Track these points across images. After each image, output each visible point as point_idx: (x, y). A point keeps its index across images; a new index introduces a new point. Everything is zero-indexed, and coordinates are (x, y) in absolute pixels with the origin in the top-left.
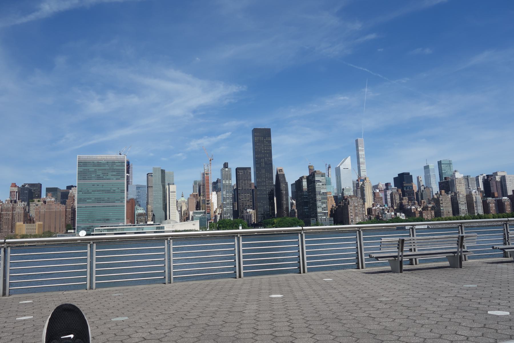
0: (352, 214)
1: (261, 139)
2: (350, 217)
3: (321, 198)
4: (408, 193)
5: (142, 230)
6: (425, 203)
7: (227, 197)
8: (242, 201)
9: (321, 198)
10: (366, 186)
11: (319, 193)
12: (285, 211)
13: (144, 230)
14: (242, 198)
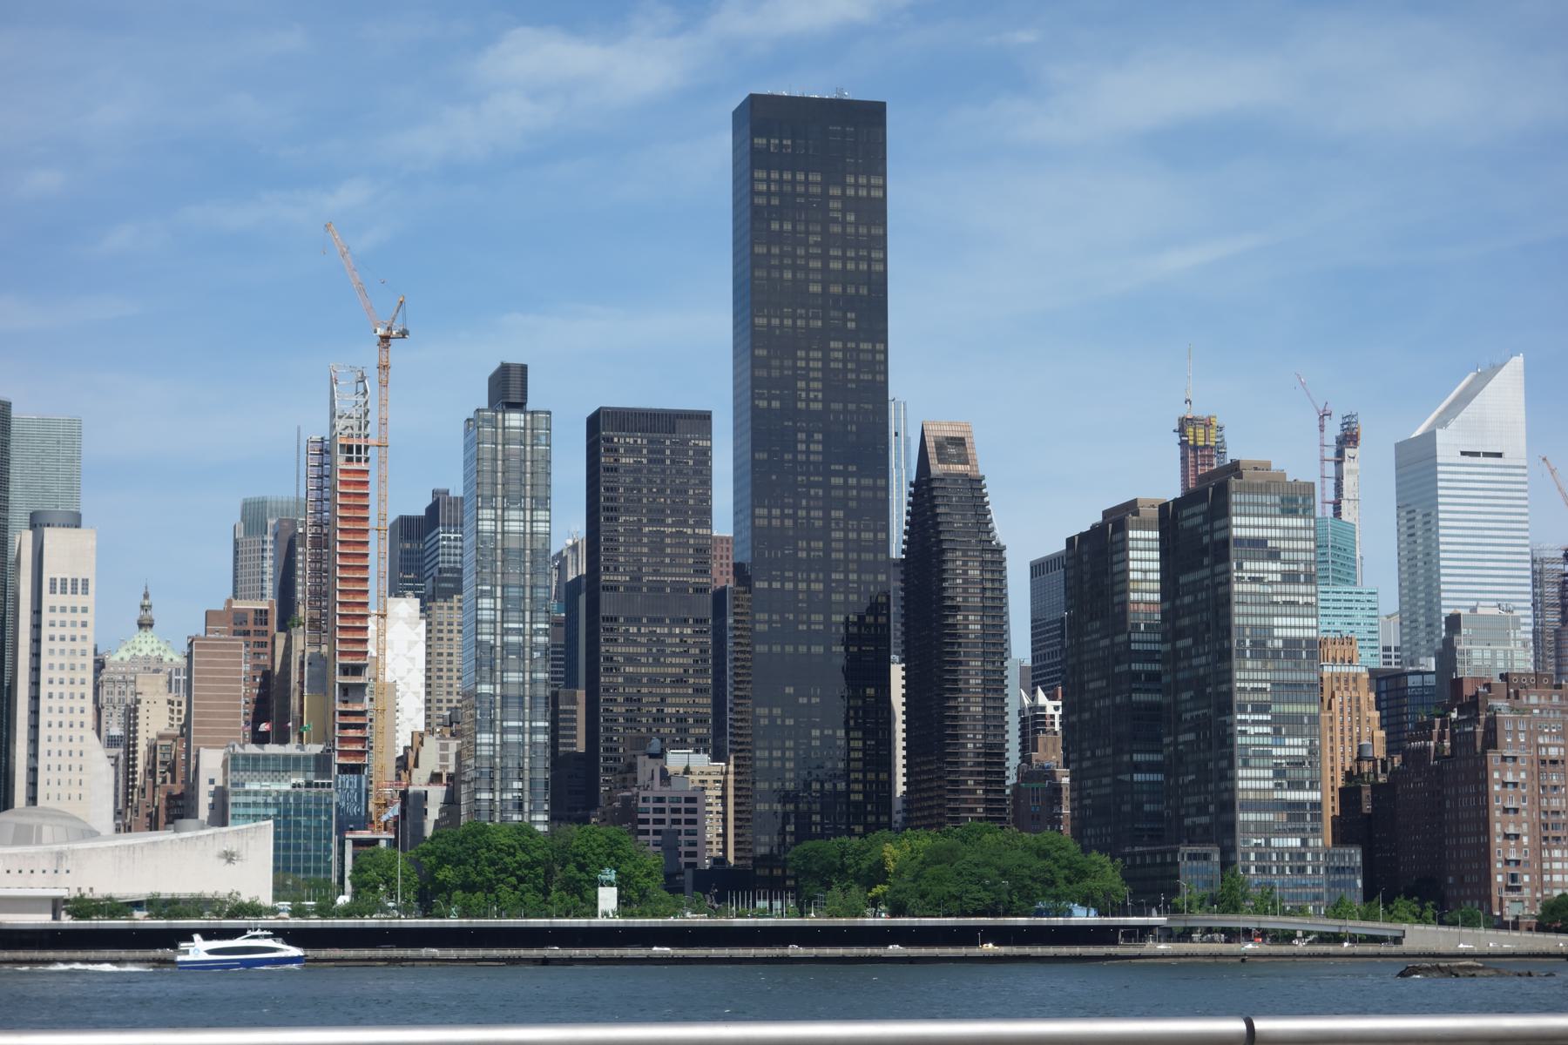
0: (1518, 825)
7: (504, 645)
8: (631, 680)
14: (631, 659)
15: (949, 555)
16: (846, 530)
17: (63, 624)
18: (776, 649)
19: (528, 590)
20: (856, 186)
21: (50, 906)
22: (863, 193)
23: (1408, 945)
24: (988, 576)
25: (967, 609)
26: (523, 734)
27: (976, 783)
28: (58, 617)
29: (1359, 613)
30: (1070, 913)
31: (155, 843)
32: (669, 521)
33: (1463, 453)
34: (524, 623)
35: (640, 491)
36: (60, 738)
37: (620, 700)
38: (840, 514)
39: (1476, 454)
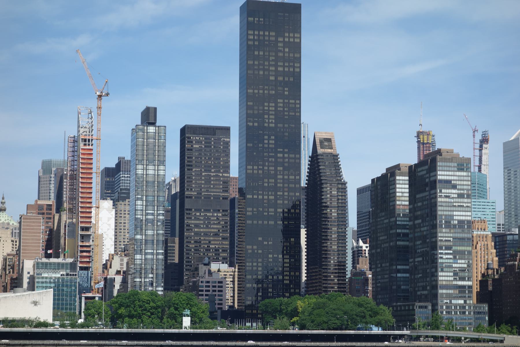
7: (146, 220)
8: (197, 234)
11: (446, 222)
12: (333, 273)
14: (197, 226)
15: (324, 186)
19: (156, 197)
20: (289, 37)
24: (340, 194)
25: (332, 207)
26: (153, 255)
27: (334, 277)
29: (488, 210)
31: (5, 297)
32: (213, 170)
34: (154, 211)
35: (201, 158)
37: (192, 242)
38: (281, 168)
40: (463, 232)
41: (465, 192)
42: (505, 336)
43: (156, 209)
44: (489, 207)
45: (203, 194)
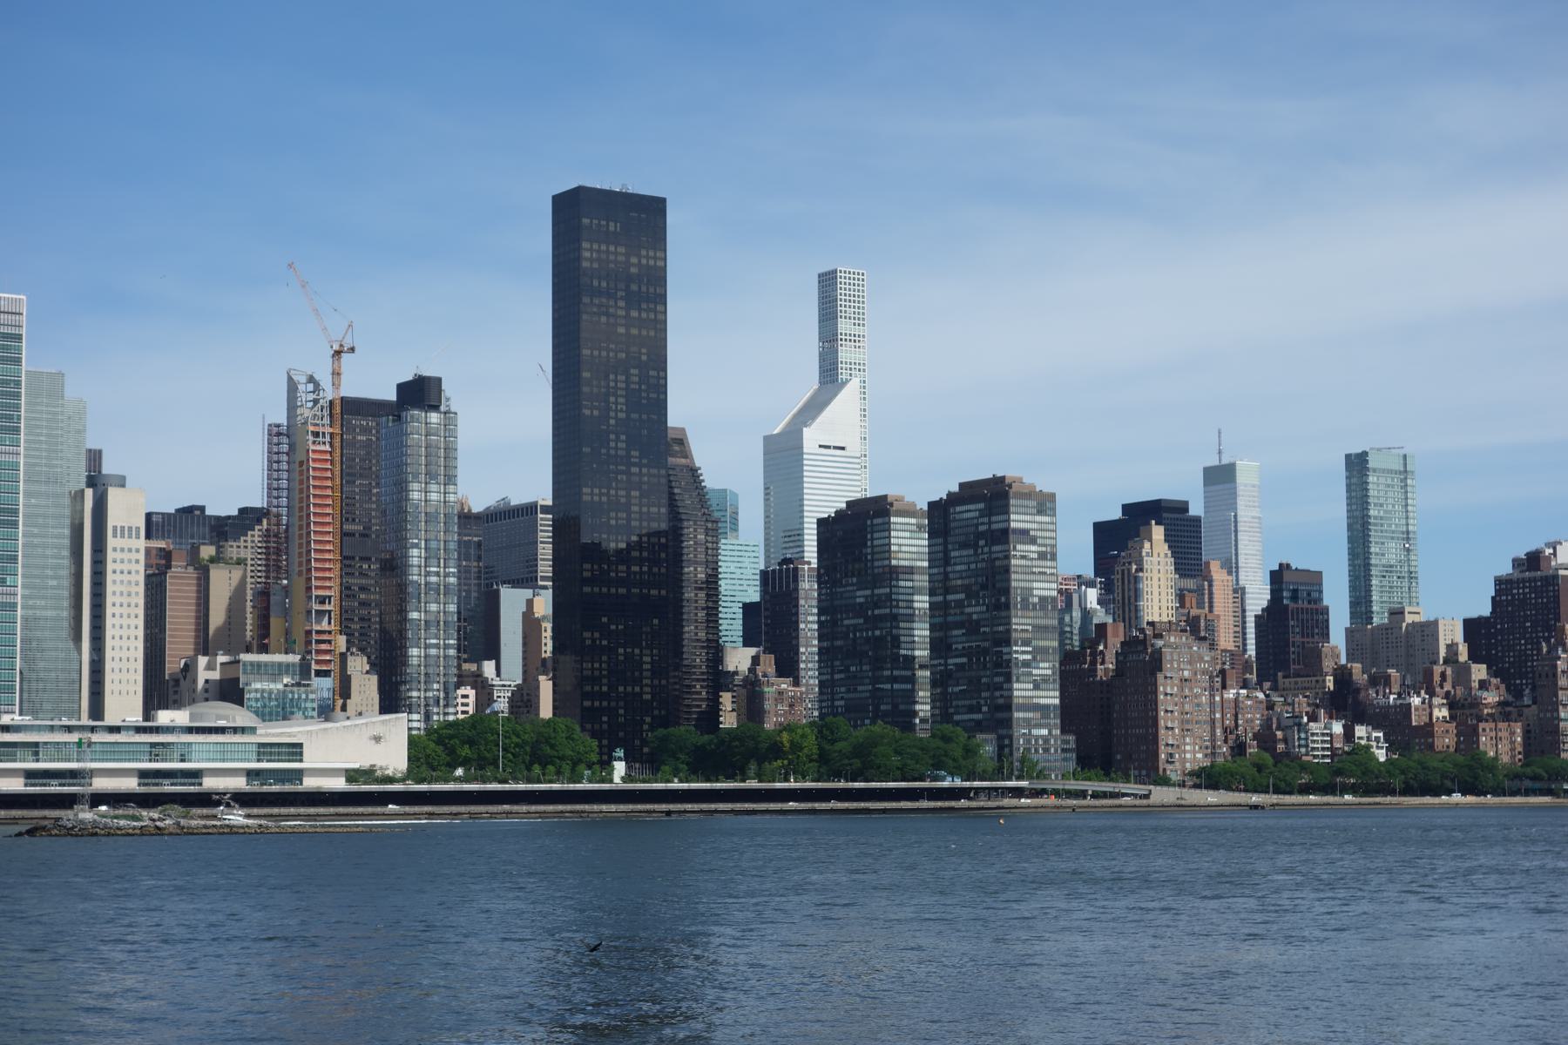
0: (1173, 721)
1: (616, 253)
2: (1161, 737)
3: (1030, 628)
4: (1303, 620)
5: (183, 761)
6: (1449, 679)
7: (427, 584)
8: (363, 604)
9: (1030, 628)
10: (1149, 575)
11: (1023, 600)
12: (698, 680)
13: (190, 761)
14: (363, 589)
16: (641, 505)
17: (122, 561)
18: (596, 590)
19: (442, 543)
20: (648, 257)
21: (245, 773)
22: (652, 262)
23: (1154, 799)
24: (710, 539)
25: (696, 563)
26: (439, 648)
27: (702, 687)
28: (119, 555)
29: (747, 560)
30: (943, 779)
31: (325, 729)
33: (820, 446)
34: (439, 566)
35: (370, 461)
36: (121, 648)
37: (356, 619)
38: (637, 493)
39: (828, 447)
40: (1046, 617)
41: (1049, 549)
42: (1151, 787)
43: (442, 565)
44: (748, 554)
45: (374, 528)
